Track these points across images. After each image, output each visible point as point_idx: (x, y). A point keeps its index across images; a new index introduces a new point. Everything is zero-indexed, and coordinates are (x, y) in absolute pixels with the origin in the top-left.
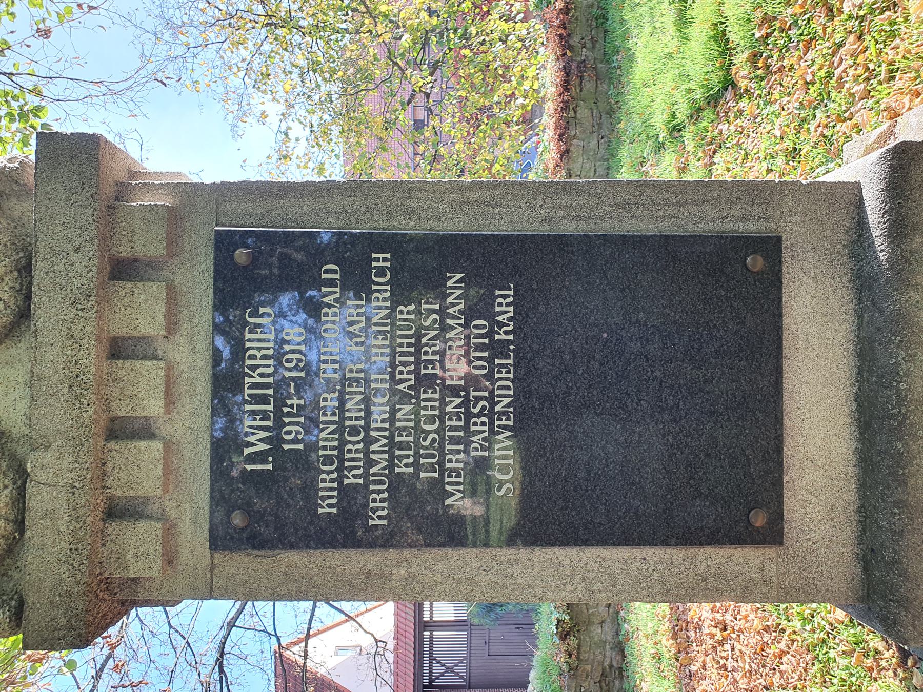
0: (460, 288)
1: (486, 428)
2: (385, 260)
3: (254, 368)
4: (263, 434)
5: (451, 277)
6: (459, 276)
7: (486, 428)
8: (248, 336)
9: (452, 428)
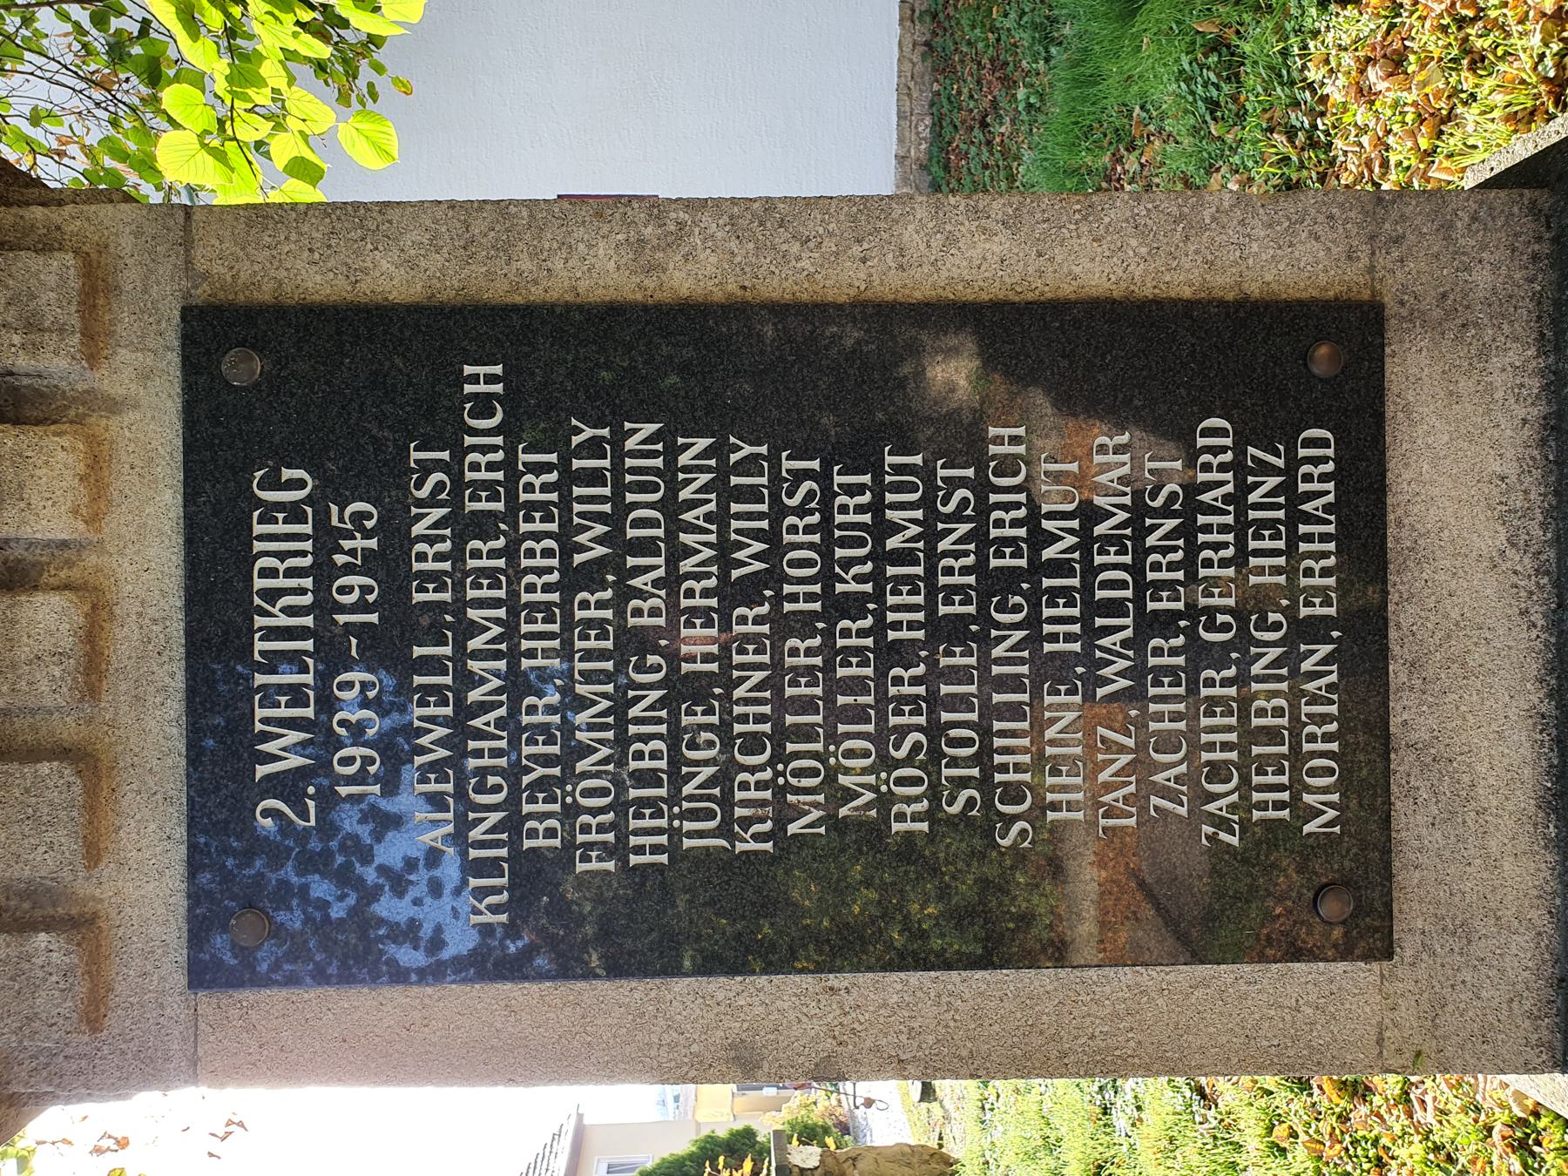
0: (708, 469)
1: (555, 562)
2: (491, 379)
3: (272, 595)
4: (294, 736)
5: (688, 446)
6: (650, 428)
7: (555, 562)
8: (258, 529)
9: (588, 655)
